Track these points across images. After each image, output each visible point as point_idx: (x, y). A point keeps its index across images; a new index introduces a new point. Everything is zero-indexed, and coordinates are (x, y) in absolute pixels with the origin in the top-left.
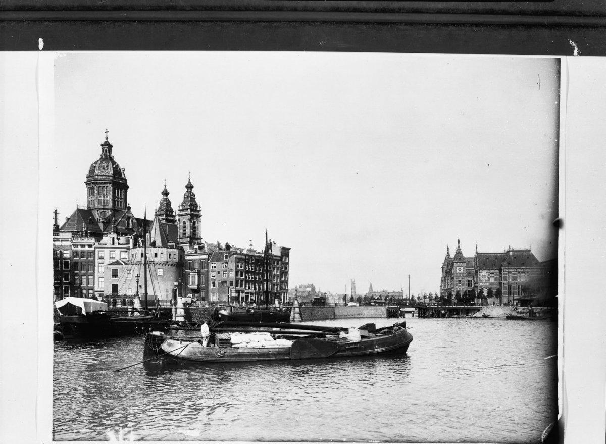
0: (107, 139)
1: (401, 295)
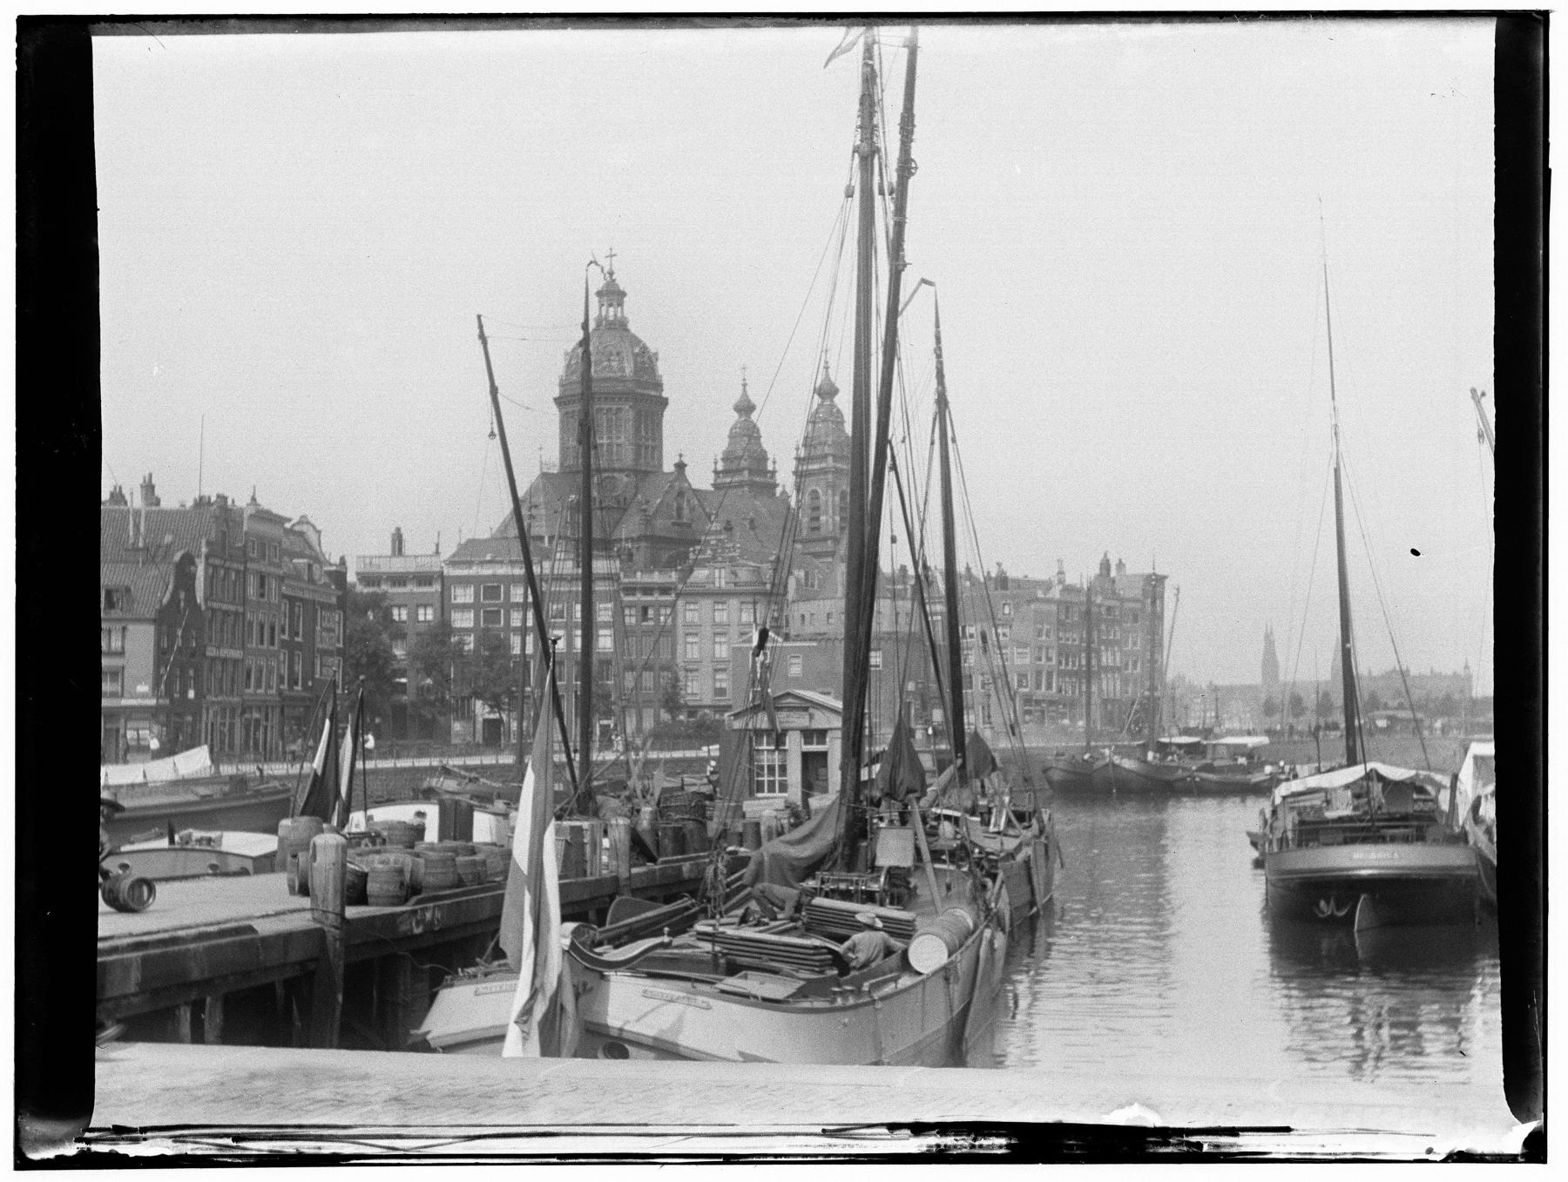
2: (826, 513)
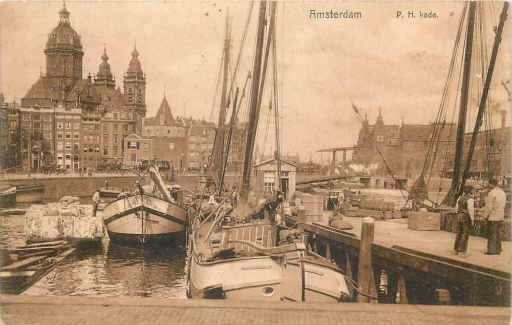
0: (64, 5)
1: (296, 159)
2: (134, 96)
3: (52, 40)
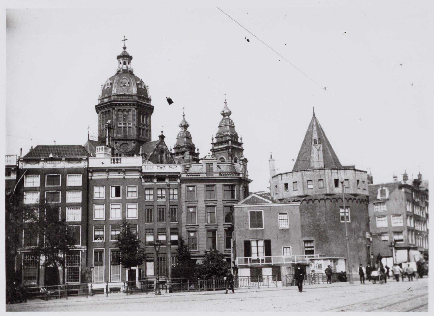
0: (125, 48)
3: (107, 92)
